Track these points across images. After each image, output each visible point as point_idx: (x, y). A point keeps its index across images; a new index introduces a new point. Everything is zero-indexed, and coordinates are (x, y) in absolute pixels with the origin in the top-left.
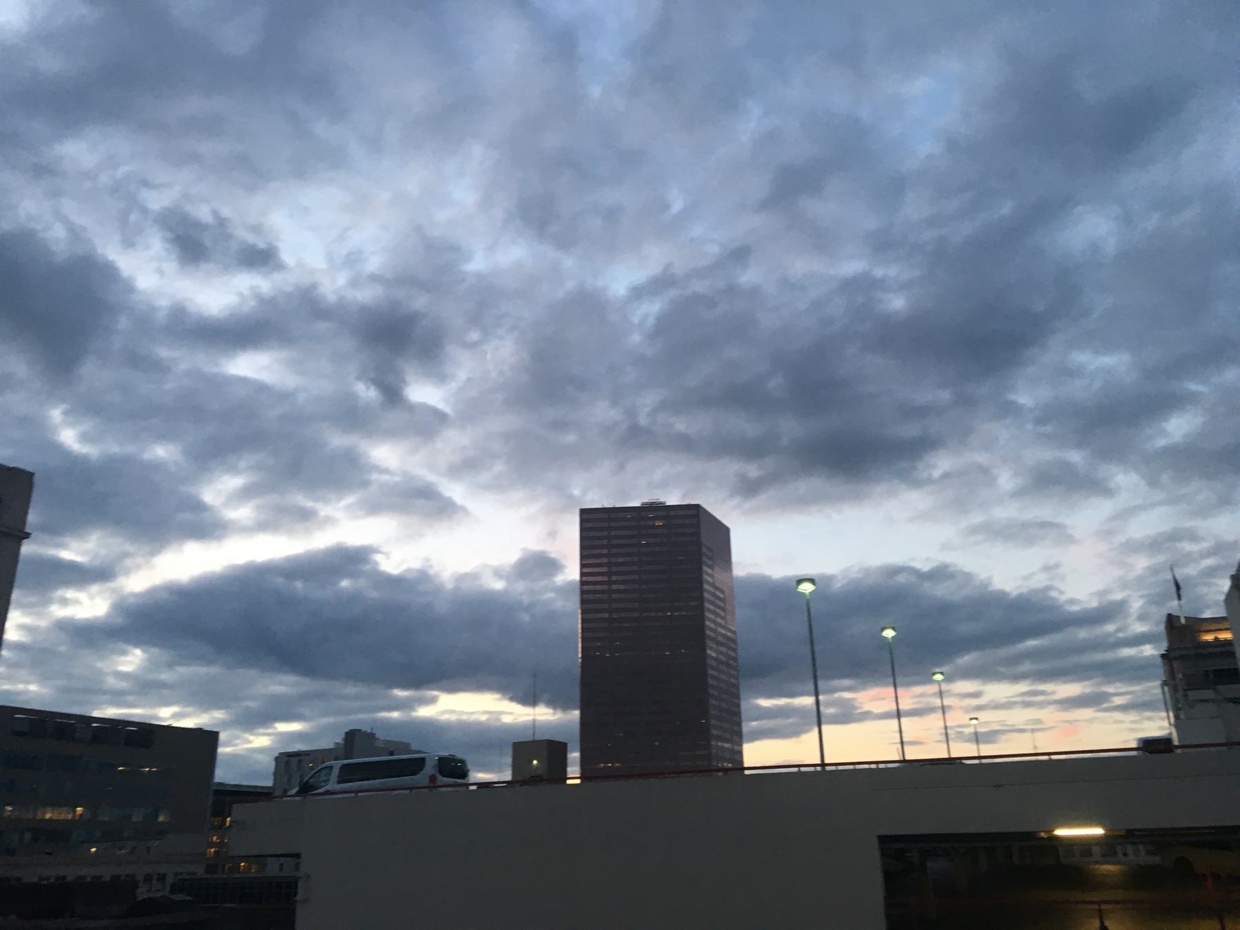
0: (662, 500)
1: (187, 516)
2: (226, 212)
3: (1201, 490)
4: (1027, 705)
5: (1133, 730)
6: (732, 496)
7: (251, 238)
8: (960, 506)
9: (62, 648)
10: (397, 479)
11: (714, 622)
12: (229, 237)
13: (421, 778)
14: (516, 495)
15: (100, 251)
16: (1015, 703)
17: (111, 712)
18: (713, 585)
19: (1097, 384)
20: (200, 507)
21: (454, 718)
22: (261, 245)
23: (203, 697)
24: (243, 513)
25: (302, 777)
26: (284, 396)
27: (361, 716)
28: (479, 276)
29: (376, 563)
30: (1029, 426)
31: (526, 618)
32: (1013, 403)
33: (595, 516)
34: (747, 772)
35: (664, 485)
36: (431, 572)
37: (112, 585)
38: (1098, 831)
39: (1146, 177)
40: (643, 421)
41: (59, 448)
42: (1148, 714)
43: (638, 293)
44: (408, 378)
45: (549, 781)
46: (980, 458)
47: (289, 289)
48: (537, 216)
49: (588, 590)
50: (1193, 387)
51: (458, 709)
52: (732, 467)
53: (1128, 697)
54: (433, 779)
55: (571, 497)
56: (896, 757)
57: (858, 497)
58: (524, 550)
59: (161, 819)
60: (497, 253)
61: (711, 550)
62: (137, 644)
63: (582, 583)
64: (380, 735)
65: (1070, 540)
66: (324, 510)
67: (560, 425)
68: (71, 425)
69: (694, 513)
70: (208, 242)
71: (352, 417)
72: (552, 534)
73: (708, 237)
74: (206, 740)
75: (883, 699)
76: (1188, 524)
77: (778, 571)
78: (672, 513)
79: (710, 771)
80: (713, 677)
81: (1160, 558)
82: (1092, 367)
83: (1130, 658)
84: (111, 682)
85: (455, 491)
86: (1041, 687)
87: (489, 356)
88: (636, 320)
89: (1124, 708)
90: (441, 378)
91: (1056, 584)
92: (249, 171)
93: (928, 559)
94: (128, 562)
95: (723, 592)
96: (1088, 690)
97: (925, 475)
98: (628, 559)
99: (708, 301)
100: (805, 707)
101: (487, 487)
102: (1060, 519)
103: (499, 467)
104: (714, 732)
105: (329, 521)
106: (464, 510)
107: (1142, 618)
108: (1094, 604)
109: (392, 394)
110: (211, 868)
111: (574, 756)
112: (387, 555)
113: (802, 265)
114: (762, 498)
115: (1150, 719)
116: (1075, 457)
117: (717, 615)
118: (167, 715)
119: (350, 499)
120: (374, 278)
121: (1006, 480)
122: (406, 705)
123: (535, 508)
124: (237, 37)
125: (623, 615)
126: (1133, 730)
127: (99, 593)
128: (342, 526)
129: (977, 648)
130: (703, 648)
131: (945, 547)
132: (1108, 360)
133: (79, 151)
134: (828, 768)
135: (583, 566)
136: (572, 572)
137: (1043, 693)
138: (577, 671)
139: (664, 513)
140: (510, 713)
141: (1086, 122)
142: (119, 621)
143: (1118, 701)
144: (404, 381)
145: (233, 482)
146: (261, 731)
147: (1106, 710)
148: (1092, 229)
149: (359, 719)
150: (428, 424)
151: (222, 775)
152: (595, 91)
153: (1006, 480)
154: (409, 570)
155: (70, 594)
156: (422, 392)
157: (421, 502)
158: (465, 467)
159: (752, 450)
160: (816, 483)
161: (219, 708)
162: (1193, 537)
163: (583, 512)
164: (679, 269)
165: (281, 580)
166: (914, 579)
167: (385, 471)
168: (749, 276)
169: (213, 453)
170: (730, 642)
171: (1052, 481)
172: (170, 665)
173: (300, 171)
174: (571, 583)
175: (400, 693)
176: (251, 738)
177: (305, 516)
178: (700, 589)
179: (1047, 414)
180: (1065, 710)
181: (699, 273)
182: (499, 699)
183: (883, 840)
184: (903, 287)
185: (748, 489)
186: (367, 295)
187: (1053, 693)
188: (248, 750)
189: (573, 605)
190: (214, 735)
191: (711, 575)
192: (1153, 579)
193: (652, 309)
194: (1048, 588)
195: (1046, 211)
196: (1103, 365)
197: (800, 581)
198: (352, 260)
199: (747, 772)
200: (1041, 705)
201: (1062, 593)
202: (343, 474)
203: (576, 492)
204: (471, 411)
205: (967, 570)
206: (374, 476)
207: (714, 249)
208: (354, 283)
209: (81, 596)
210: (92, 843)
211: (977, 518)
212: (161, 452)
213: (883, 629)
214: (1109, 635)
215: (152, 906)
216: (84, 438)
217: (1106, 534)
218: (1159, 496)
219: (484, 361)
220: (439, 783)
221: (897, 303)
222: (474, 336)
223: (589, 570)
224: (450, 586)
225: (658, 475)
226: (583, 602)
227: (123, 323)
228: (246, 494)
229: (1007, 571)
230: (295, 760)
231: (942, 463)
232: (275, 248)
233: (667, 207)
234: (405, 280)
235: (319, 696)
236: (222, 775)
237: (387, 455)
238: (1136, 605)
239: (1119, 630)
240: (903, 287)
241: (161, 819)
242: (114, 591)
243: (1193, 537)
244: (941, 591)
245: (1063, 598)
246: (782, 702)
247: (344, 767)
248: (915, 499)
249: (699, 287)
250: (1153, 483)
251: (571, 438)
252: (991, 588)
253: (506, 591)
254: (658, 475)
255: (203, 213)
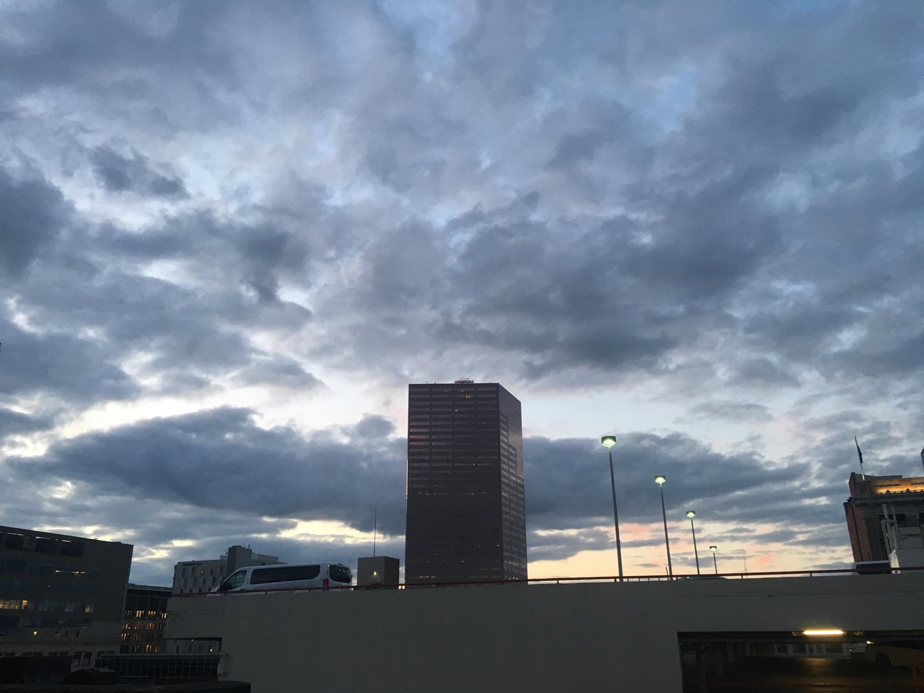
0: (471, 379)
1: (111, 382)
2: (146, 153)
3: (863, 384)
4: (734, 539)
5: (811, 559)
6: (521, 377)
7: (162, 173)
8: (689, 391)
9: (11, 480)
10: (270, 359)
11: (508, 472)
12: (145, 171)
13: (318, 580)
14: (360, 374)
15: (47, 178)
16: (726, 537)
17: (47, 529)
18: (507, 444)
19: (791, 304)
20: (121, 376)
21: (308, 539)
22: (170, 178)
23: (118, 519)
24: (152, 381)
25: (224, 578)
26: (186, 294)
27: (237, 536)
28: (336, 209)
29: (253, 422)
30: (740, 334)
31: (364, 465)
32: (731, 316)
33: (418, 390)
34: (530, 583)
35: (471, 368)
36: (294, 429)
37: (49, 432)
38: (839, 632)
39: (829, 155)
40: (456, 321)
41: (13, 328)
42: (823, 548)
43: (455, 225)
44: (279, 283)
45: (386, 586)
46: (706, 356)
47: (191, 212)
48: (382, 167)
49: (414, 445)
50: (861, 309)
51: (311, 533)
52: (521, 357)
53: (809, 535)
54: (326, 582)
55: (401, 377)
56: (662, 571)
57: (614, 382)
58: (365, 414)
59: (87, 610)
60: (353, 194)
61: (507, 418)
62: (69, 477)
63: (410, 440)
64: (256, 551)
65: (769, 418)
66: (215, 381)
67: (393, 322)
68: (24, 311)
69: (495, 389)
70: (129, 174)
71: (239, 312)
72: (387, 403)
73: (508, 186)
74: (123, 551)
75: (630, 532)
76: (854, 409)
77: (555, 435)
78: (479, 389)
79: (504, 582)
80: (507, 513)
81: (834, 434)
82: (786, 292)
83: (811, 507)
84: (48, 506)
85: (314, 369)
86: (746, 526)
87: (342, 271)
88: (451, 245)
89: (805, 543)
90: (306, 284)
91: (758, 450)
92: (162, 122)
93: (666, 429)
94: (63, 416)
95: (515, 449)
96: (779, 529)
97: (664, 366)
98: (446, 423)
99: (506, 233)
100: (571, 537)
101: (338, 367)
102: (760, 403)
103: (348, 352)
104: (506, 554)
105: (219, 389)
106: (321, 383)
107: (819, 477)
108: (786, 465)
109: (267, 295)
110: (124, 649)
111: (402, 570)
112: (262, 416)
113: (576, 210)
114: (543, 381)
115: (823, 551)
116: (773, 358)
117: (510, 467)
118: (89, 532)
119: (235, 373)
120: (256, 207)
121: (722, 373)
122: (274, 529)
123: (375, 383)
124: (159, 24)
125: (440, 464)
126: (811, 559)
127: (41, 438)
128: (227, 393)
129: (697, 497)
130: (499, 490)
131: (678, 421)
132: (797, 288)
133: (35, 104)
134: (625, 580)
135: (410, 427)
136: (402, 432)
137: (747, 530)
138: (405, 505)
139: (473, 389)
140: (352, 537)
141: (787, 111)
142: (55, 460)
143: (801, 537)
144: (277, 285)
145: (144, 358)
146: (162, 546)
147: (792, 544)
148: (788, 192)
149: (236, 539)
150: (295, 319)
151: (134, 578)
152: (428, 76)
153: (722, 373)
154: (277, 428)
155: (18, 438)
156: (291, 294)
157: (289, 377)
158: (322, 351)
159: (535, 344)
160: (583, 370)
161: (129, 528)
162: (857, 418)
163: (413, 388)
164: (486, 208)
165: (180, 432)
166: (654, 443)
167: (262, 353)
168: (536, 216)
169: (131, 335)
170: (519, 488)
171: (756, 374)
172: (94, 494)
173: (203, 127)
174: (400, 441)
175: (267, 519)
176: (154, 551)
177: (200, 384)
178: (499, 446)
179: (755, 325)
180: (761, 544)
181: (500, 212)
182: (343, 526)
183: (681, 635)
184: (651, 228)
185: (533, 373)
186: (250, 221)
187: (754, 530)
188: (154, 560)
189: (402, 457)
190: (130, 547)
191: (507, 438)
192: (827, 449)
193: (463, 238)
194: (753, 453)
195: (758, 175)
196: (794, 291)
197: (604, 439)
198: (241, 192)
199: (530, 583)
200: (745, 539)
201: (763, 457)
202: (229, 354)
203: (406, 373)
204: (328, 310)
205: (694, 438)
206: (253, 356)
207: (513, 195)
208: (242, 211)
209: (27, 440)
210: (34, 626)
211: (701, 400)
212: (91, 333)
213: (656, 477)
214: (795, 489)
215: (83, 677)
216: (32, 321)
217: (794, 414)
218: (833, 388)
219: (344, 271)
220: (330, 586)
221: (646, 239)
222: (332, 253)
223: (415, 430)
224: (308, 440)
225: (467, 362)
226: (410, 454)
227: (64, 234)
228: (156, 366)
229: (722, 439)
230: (190, 568)
231: (676, 359)
232: (181, 181)
233: (478, 164)
234: (281, 210)
235: (201, 521)
236: (134, 578)
237: (263, 341)
238: (816, 467)
239: (803, 485)
240: (651, 228)
241: (87, 610)
242: (52, 436)
243: (857, 418)
244: (674, 453)
245: (763, 461)
246: (555, 532)
247: (255, 571)
248: (658, 385)
249: (500, 222)
250: (829, 378)
251: (402, 332)
252: (711, 452)
253: (348, 447)
254: (467, 362)
255: (127, 154)
